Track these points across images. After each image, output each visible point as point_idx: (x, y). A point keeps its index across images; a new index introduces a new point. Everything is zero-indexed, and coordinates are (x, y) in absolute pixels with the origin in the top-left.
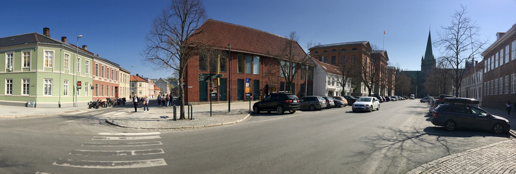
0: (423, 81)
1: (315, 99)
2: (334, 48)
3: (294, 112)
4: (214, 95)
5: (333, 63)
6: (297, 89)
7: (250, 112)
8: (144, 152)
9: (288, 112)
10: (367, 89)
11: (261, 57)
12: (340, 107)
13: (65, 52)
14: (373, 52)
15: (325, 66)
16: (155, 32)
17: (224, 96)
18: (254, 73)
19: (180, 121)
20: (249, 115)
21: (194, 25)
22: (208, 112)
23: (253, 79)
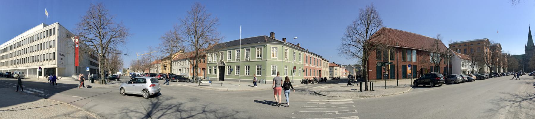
0: (528, 61)
1: (454, 76)
2: (465, 44)
3: (441, 85)
5: (465, 53)
6: (442, 70)
7: (411, 86)
8: (344, 112)
10: (488, 68)
11: (417, 51)
12: (471, 81)
13: (285, 48)
16: (348, 35)
17: (393, 76)
19: (365, 92)
21: (373, 31)
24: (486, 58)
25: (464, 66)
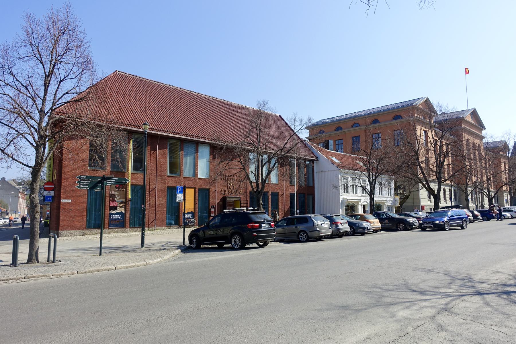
3: (265, 244)
4: (119, 217)
9: (255, 245)
12: (363, 234)
14: (440, 118)
15: (337, 156)
18: (200, 176)
20: (179, 250)
22: (96, 249)
23: (198, 186)
24: (419, 162)
25: (349, 190)
